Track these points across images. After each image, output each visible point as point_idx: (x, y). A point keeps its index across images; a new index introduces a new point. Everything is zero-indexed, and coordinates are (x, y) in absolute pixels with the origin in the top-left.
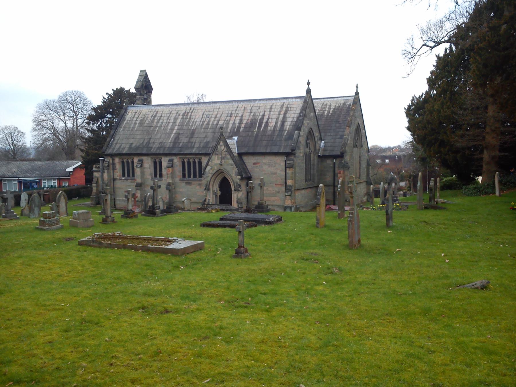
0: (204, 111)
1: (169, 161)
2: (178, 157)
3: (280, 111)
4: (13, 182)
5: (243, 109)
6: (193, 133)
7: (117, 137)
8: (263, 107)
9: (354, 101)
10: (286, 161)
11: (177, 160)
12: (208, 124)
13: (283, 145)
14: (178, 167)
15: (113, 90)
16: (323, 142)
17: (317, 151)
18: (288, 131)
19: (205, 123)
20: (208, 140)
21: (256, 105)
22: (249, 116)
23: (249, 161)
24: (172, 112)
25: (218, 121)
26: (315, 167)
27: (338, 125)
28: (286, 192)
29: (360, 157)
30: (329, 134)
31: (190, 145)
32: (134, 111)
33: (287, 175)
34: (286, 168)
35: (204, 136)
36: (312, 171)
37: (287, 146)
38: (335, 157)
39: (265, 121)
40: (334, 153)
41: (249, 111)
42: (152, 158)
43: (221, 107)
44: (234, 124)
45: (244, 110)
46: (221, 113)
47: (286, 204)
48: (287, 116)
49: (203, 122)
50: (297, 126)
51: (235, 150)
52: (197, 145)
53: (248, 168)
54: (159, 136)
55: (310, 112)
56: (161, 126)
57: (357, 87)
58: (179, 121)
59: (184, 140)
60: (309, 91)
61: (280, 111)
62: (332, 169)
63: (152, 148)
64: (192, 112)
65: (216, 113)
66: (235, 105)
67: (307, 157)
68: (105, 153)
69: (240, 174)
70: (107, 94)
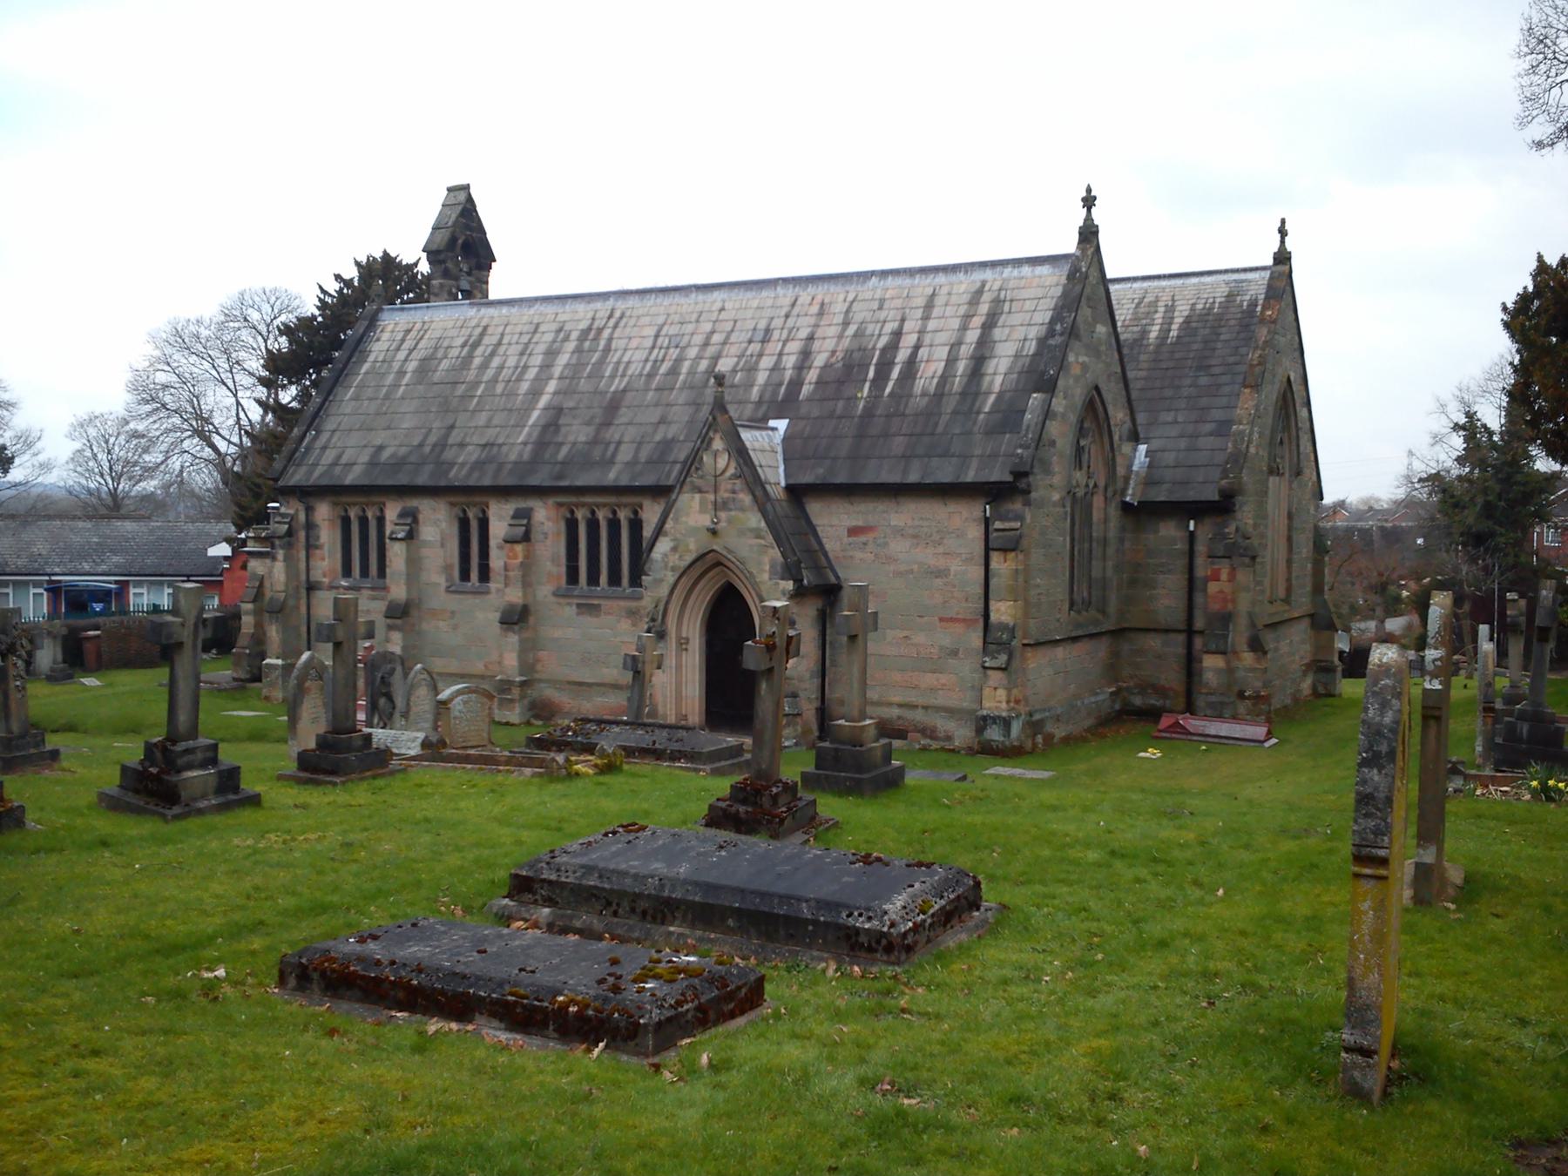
0: (661, 320)
1: (514, 517)
2: (551, 501)
3: (968, 317)
4: (33, 591)
5: (815, 309)
6: (613, 406)
7: (330, 425)
8: (898, 303)
9: (1270, 287)
10: (987, 522)
11: (545, 515)
12: (674, 371)
13: (978, 452)
14: (548, 542)
15: (358, 264)
16: (1143, 448)
17: (1120, 484)
18: (1001, 394)
19: (664, 369)
20: (672, 431)
21: (868, 295)
22: (840, 337)
23: (832, 522)
24: (542, 328)
25: (716, 359)
26: (1111, 551)
27: (1204, 380)
28: (985, 651)
29: (1290, 516)
30: (1169, 417)
31: (597, 453)
32: (402, 327)
33: (993, 582)
34: (987, 550)
35: (655, 419)
36: (1096, 565)
37: (994, 456)
38: (1198, 510)
39: (902, 355)
40: (1192, 495)
41: (839, 319)
42: (452, 504)
43: (727, 306)
44: (777, 368)
45: (821, 314)
46: (728, 326)
47: (986, 704)
48: (998, 333)
49: (655, 368)
50: (1041, 374)
51: (776, 475)
52: (625, 454)
53: (827, 547)
54: (482, 419)
55: (1096, 321)
56: (495, 380)
57: (1283, 232)
58: (563, 359)
59: (576, 433)
60: (1089, 234)
61: (968, 317)
62: (1182, 563)
63: (452, 464)
64: (616, 326)
65: (708, 327)
66: (785, 295)
67: (1079, 505)
68: (281, 483)
69: (790, 570)
70: (338, 277)
